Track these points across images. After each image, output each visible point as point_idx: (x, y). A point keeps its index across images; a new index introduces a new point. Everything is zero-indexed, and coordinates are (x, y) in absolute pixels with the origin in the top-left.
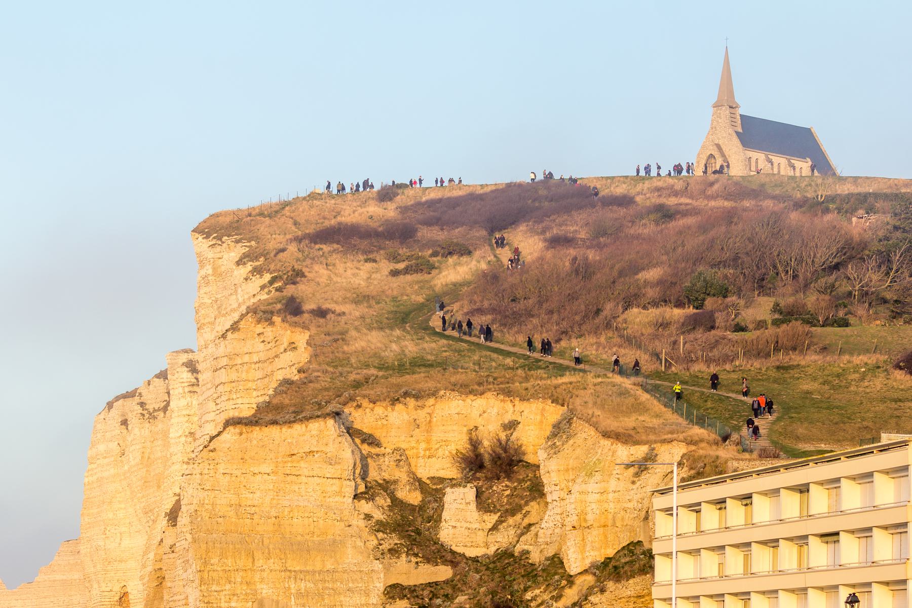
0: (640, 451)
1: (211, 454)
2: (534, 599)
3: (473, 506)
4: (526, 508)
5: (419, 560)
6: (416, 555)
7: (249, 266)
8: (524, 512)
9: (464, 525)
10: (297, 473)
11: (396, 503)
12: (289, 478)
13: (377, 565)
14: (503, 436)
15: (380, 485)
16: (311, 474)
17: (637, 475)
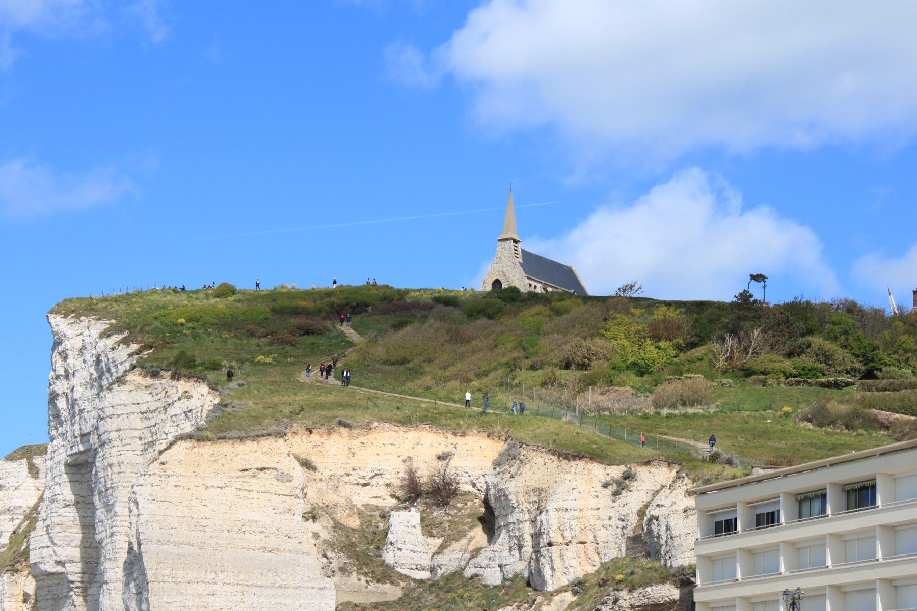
0: (616, 472)
1: (162, 466)
3: (419, 530)
5: (369, 579)
6: (366, 574)
7: (116, 338)
8: (469, 536)
9: (410, 544)
10: (250, 488)
11: (337, 526)
12: (243, 493)
15: (322, 508)
16: (263, 489)
17: (616, 494)
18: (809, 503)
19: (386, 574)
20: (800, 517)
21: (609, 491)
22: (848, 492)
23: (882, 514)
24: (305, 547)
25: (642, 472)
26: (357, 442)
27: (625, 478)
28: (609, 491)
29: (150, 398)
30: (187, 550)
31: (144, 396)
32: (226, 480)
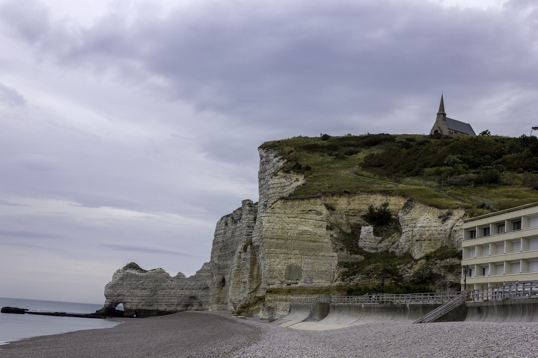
0: (445, 212)
2: (400, 268)
3: (372, 234)
4: (393, 235)
6: (350, 251)
11: (342, 232)
13: (335, 254)
14: (383, 208)
18: (486, 231)
19: (358, 251)
20: (498, 232)
21: (441, 220)
22: (514, 223)
23: (525, 232)
24: (326, 240)
25: (455, 212)
26: (351, 199)
27: (448, 215)
28: (441, 220)
29: (285, 181)
30: (281, 241)
31: (284, 180)
32: (296, 215)
